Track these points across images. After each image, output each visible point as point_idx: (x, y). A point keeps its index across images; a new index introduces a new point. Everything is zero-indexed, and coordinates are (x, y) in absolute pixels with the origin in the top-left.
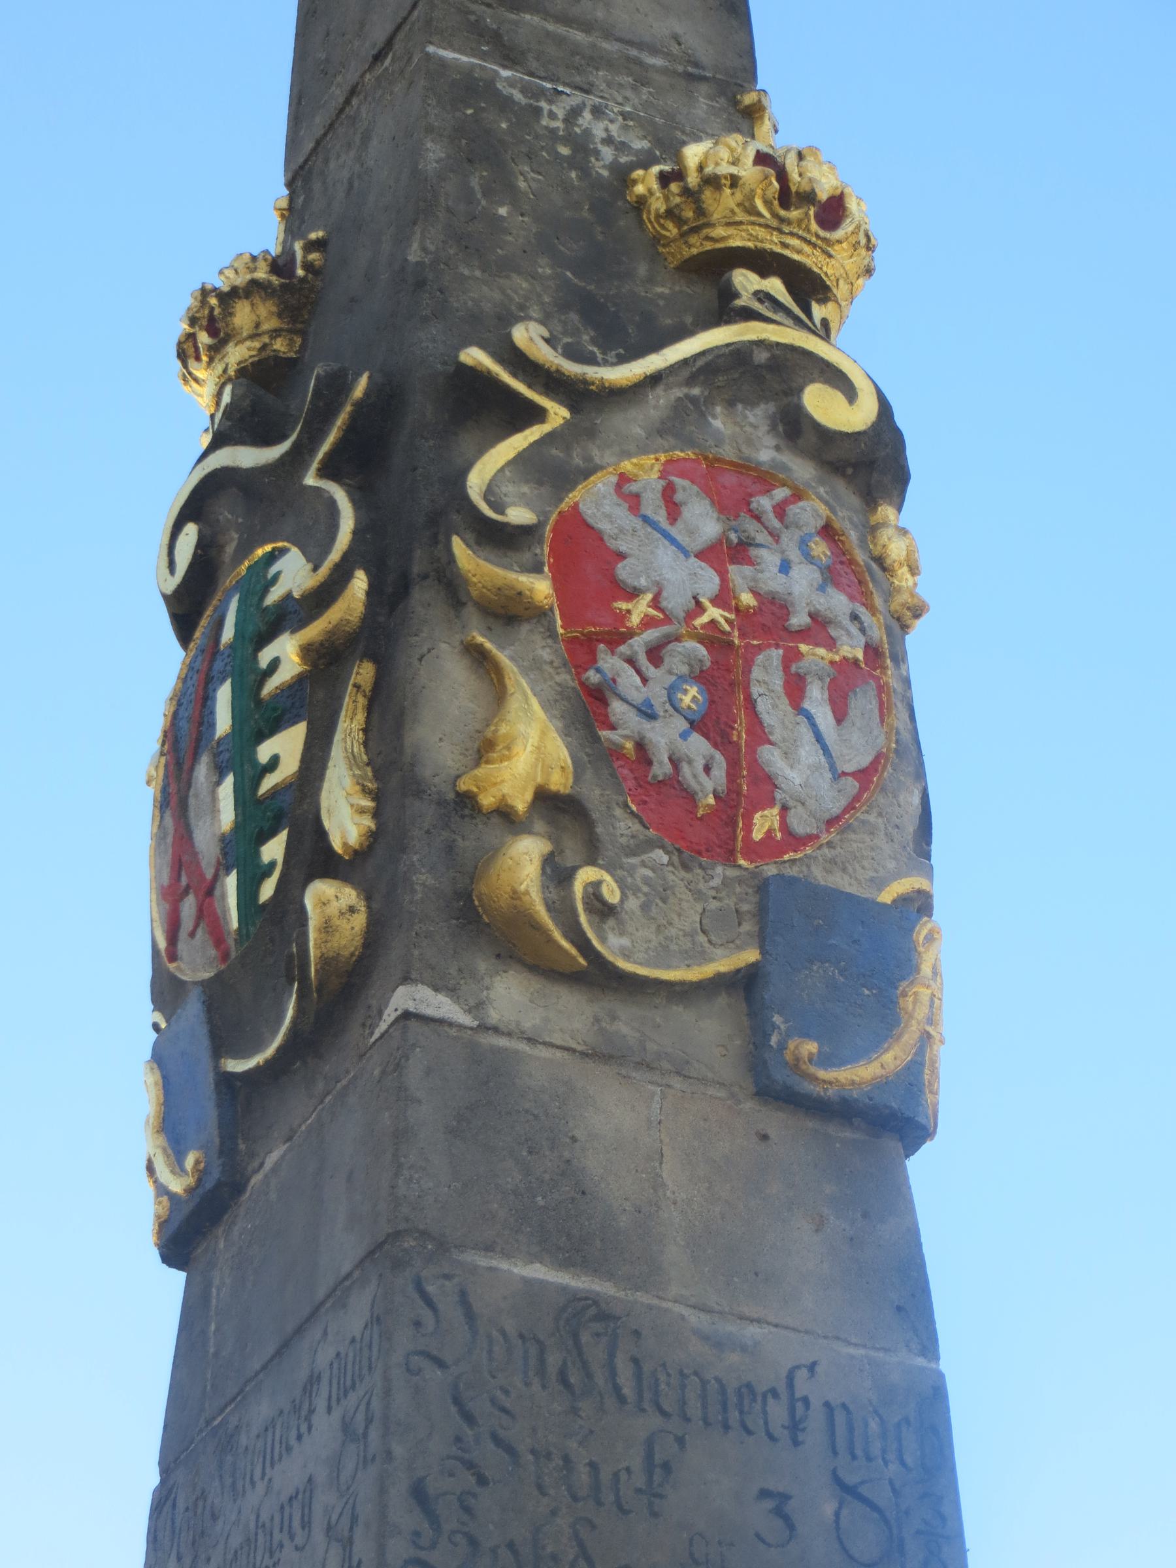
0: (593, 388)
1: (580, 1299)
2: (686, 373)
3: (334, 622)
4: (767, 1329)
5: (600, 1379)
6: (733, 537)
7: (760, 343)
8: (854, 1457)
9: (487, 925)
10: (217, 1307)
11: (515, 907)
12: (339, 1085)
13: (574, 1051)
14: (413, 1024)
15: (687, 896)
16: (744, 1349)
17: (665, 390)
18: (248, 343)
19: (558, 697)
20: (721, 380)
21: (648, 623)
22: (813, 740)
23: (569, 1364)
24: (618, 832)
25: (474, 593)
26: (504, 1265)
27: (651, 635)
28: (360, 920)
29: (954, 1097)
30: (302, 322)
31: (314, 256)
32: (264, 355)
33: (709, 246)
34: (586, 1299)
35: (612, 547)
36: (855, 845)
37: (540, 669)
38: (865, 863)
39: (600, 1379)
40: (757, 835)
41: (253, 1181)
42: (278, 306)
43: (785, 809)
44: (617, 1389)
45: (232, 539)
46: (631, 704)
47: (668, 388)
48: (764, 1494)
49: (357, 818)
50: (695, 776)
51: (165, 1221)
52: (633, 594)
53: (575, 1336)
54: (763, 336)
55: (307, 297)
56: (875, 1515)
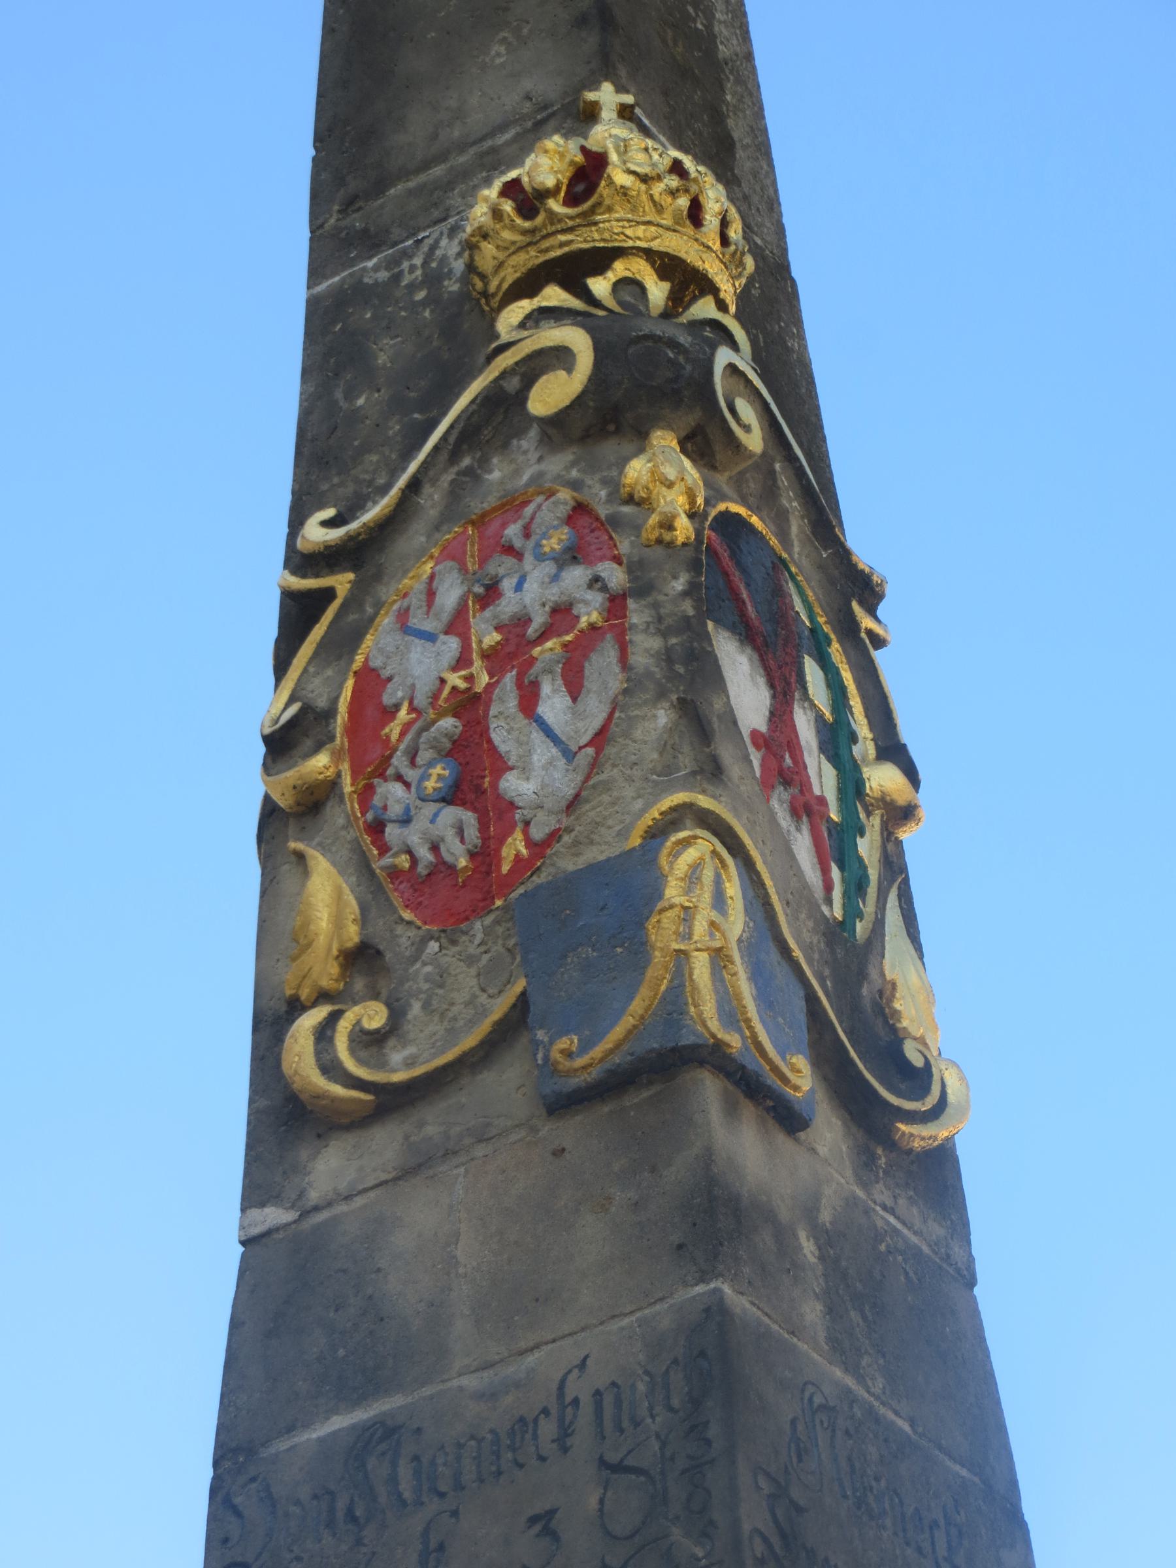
1: (369, 1428)
2: (444, 456)
4: (546, 1348)
7: (504, 375)
8: (622, 1431)
13: (386, 1182)
16: (517, 1385)
17: (433, 485)
20: (487, 433)
22: (544, 738)
23: (356, 1499)
34: (375, 1424)
36: (592, 814)
38: (610, 822)
47: (434, 482)
56: (642, 1479)
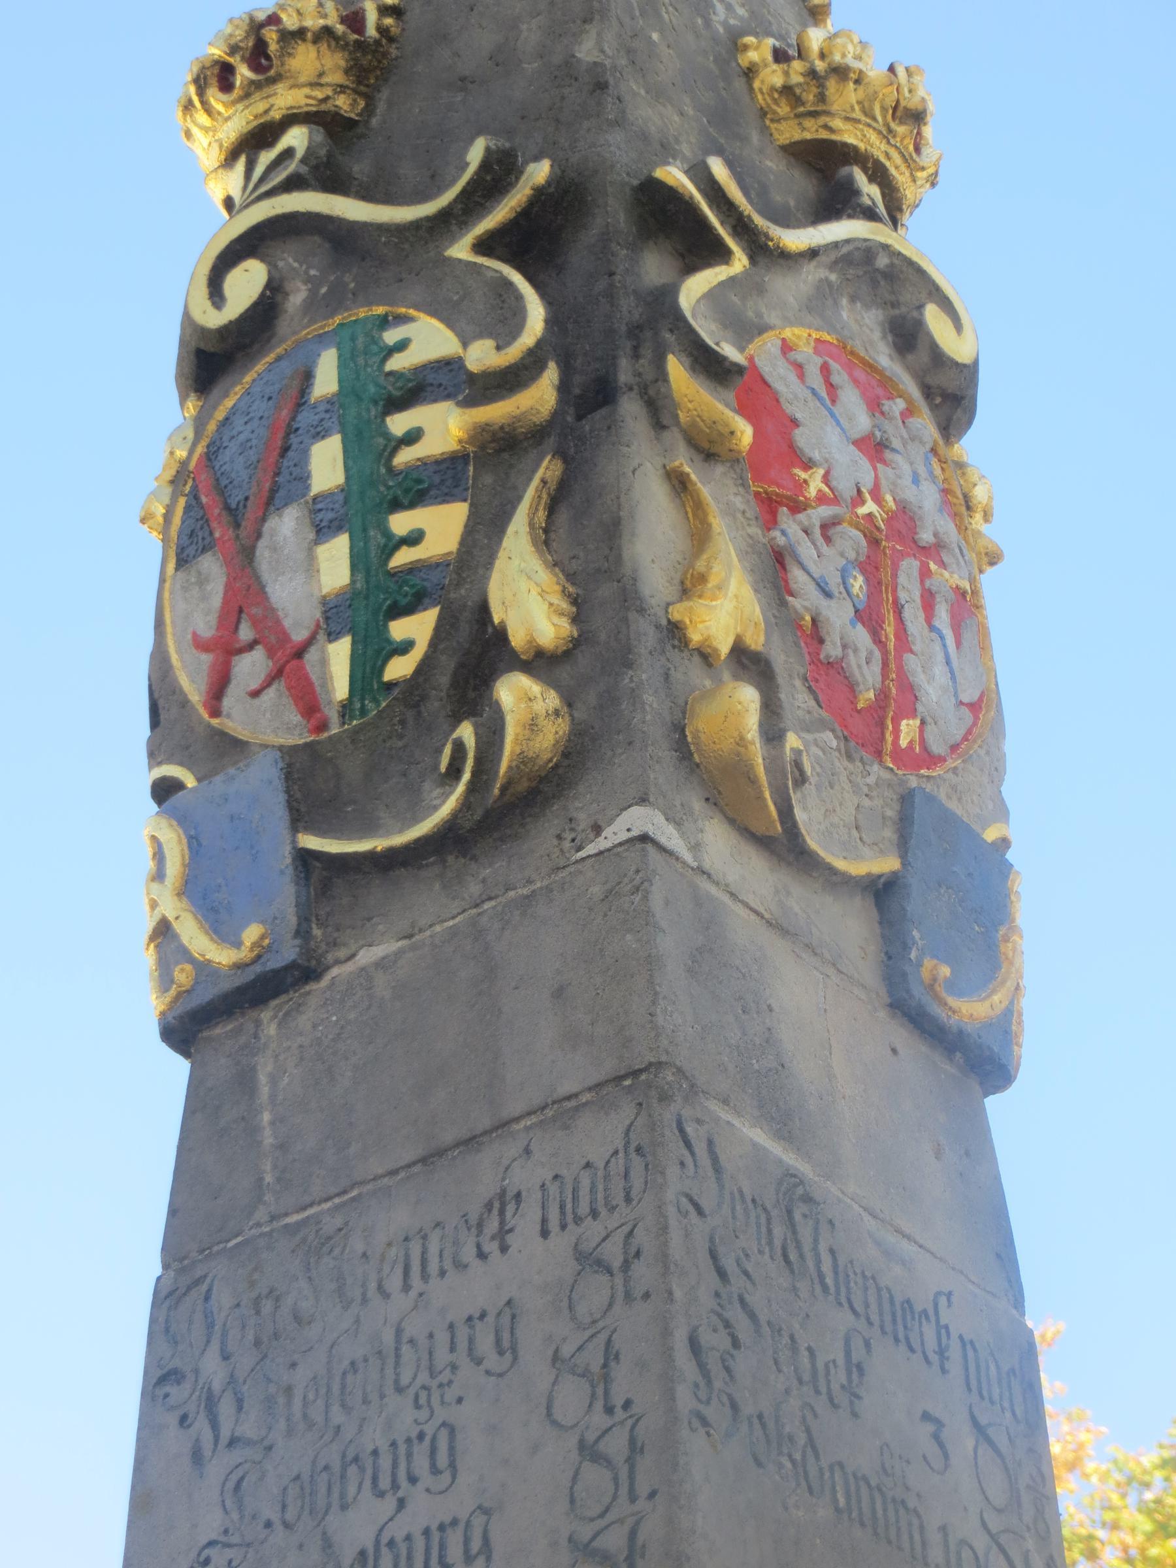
0: (770, 244)
2: (833, 256)
3: (523, 409)
5: (811, 1264)
6: (878, 434)
9: (698, 765)
10: (273, 1097)
11: (738, 754)
12: (512, 894)
14: (649, 847)
15: (847, 786)
18: (307, 91)
19: (749, 550)
21: (821, 499)
24: (797, 704)
25: (682, 416)
26: (736, 1122)
27: (825, 511)
28: (562, 726)
29: (1035, 1052)
30: (367, 86)
31: (388, 21)
32: (323, 107)
33: (824, 135)
35: (788, 411)
37: (734, 517)
39: (811, 1264)
40: (904, 743)
41: (335, 971)
42: (347, 61)
43: (923, 722)
44: (821, 1277)
45: (299, 290)
46: (812, 577)
48: (926, 1416)
49: (556, 620)
50: (859, 667)
51: (187, 991)
52: (808, 465)
53: (789, 1212)
54: (889, 242)
55: (380, 62)
